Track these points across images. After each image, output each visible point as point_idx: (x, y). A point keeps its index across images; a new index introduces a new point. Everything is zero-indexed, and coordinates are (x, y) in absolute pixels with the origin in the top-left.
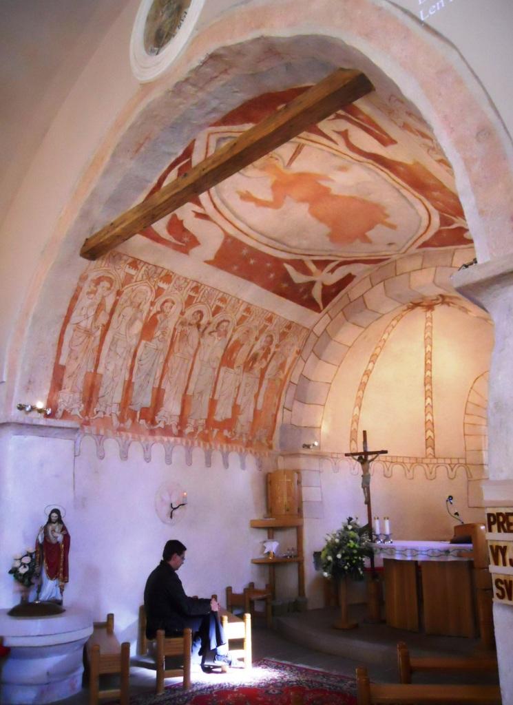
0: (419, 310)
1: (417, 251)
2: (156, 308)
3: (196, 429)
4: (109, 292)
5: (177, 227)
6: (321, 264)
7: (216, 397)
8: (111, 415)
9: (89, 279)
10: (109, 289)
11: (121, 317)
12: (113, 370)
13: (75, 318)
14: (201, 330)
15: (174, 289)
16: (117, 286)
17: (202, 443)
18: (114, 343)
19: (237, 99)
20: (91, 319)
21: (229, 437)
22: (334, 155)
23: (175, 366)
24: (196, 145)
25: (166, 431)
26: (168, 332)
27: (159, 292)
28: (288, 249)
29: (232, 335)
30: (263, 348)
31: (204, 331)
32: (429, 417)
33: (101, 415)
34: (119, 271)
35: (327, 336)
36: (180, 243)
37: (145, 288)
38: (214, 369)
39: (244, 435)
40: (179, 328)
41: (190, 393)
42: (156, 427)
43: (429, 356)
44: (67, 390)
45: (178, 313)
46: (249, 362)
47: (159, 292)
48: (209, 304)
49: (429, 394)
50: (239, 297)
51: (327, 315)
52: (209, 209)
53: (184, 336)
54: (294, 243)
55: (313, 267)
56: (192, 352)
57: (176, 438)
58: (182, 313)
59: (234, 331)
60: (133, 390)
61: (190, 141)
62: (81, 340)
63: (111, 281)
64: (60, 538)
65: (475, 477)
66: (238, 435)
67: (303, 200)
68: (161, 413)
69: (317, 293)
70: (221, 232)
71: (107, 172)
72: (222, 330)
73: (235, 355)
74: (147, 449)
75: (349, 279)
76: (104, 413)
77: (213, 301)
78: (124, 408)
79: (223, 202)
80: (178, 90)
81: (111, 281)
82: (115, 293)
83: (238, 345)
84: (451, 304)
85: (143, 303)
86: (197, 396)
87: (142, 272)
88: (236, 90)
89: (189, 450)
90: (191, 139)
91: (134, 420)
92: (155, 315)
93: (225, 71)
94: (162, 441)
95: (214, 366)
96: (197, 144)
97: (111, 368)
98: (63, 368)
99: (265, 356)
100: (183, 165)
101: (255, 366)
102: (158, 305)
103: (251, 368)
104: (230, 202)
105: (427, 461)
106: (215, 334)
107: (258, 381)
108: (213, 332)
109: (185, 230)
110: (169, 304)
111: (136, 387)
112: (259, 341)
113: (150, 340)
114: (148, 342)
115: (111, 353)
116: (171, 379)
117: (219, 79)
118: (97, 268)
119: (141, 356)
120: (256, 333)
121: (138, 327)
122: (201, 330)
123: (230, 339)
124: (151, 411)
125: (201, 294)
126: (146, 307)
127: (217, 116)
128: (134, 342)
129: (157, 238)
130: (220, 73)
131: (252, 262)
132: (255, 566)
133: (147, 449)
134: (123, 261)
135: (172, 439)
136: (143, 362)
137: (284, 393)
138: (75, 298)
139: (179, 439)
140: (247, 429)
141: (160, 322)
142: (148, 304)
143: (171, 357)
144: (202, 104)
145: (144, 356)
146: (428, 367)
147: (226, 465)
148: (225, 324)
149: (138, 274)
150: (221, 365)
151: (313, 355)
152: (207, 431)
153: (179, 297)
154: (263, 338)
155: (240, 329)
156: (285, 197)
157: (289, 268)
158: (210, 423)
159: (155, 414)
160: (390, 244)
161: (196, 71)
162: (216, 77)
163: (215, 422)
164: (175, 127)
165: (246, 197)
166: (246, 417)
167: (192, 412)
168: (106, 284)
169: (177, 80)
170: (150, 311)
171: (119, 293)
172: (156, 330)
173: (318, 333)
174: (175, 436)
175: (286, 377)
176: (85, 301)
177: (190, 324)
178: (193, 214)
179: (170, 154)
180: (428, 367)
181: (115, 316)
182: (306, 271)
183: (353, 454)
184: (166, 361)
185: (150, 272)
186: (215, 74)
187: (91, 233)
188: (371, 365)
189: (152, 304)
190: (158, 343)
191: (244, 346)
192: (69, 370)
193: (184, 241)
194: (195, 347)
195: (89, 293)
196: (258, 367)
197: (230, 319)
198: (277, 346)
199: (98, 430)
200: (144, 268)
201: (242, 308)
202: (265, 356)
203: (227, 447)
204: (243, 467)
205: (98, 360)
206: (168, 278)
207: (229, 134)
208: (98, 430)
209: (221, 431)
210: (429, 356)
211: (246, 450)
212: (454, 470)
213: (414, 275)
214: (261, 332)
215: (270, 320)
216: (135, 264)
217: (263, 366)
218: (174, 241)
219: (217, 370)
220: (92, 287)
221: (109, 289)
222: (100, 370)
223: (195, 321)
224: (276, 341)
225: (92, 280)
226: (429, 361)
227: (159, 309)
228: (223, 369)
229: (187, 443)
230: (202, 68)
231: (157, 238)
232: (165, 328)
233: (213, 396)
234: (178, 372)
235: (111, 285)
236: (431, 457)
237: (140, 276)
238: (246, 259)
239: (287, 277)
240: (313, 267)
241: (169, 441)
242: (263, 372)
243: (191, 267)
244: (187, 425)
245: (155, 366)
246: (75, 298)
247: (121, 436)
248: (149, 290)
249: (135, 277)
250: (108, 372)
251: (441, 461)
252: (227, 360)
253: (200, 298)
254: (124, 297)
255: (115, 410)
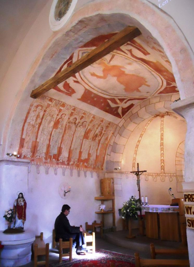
0: (158, 117)
1: (158, 95)
2: (59, 117)
3: (74, 162)
4: (41, 110)
5: (67, 86)
6: (121, 100)
7: (82, 150)
8: (42, 157)
9: (34, 106)
10: (41, 109)
11: (46, 120)
12: (43, 140)
13: (28, 120)
14: (76, 125)
15: (66, 110)
16: (44, 108)
17: (76, 168)
18: (43, 130)
19: (90, 37)
20: (34, 121)
21: (87, 165)
22: (126, 59)
23: (66, 138)
24: (74, 55)
25: (63, 163)
26: (64, 126)
27: (60, 110)
28: (109, 94)
29: (88, 127)
30: (100, 132)
31: (77, 125)
32: (162, 158)
33: (38, 157)
34: (45, 103)
35: (124, 127)
36: (68, 92)
37: (55, 109)
38: (81, 140)
39: (92, 165)
40: (68, 124)
41: (72, 149)
42: (59, 162)
43: (162, 135)
44: (26, 148)
45: (67, 119)
46: (94, 137)
47: (60, 110)
48: (79, 115)
49: (162, 149)
50: (90, 113)
51: (124, 119)
52: (79, 79)
53: (70, 127)
54: (111, 92)
55: (118, 101)
56: (73, 133)
57: (67, 166)
58: (69, 119)
59: (89, 125)
60: (50, 148)
61: (72, 53)
62: (31, 129)
63: (42, 106)
64: (23, 204)
65: (180, 181)
66: (90, 165)
67: (114, 76)
68: (61, 157)
69: (120, 111)
70: (84, 88)
71: (40, 65)
72: (84, 125)
73: (89, 134)
74: (55, 170)
75: (132, 106)
76: (39, 157)
77: (81, 114)
78: (47, 154)
79: (84, 76)
80: (67, 34)
81: (42, 106)
82: (43, 111)
83: (90, 131)
84: (171, 115)
85: (54, 115)
86: (74, 150)
87: (54, 103)
88: (89, 34)
89: (71, 170)
90: (72, 53)
91: (51, 159)
92: (59, 119)
93: (85, 27)
94: (61, 167)
95: (81, 139)
96: (75, 54)
97: (42, 139)
98: (24, 139)
99: (100, 135)
100: (69, 62)
101: (96, 138)
102: (60, 116)
103: (95, 139)
104: (87, 77)
105: (162, 175)
106: (81, 127)
107: (97, 144)
108: (81, 126)
109: (70, 87)
110: (64, 115)
111: (51, 147)
112: (98, 129)
113: (57, 129)
114: (56, 130)
115: (42, 134)
116: (65, 144)
117: (83, 30)
118: (37, 101)
119: (53, 135)
120: (97, 126)
121: (52, 124)
122: (76, 125)
123: (87, 128)
124: (57, 156)
125: (76, 111)
126: (55, 116)
127: (82, 44)
128: (51, 129)
129: (59, 90)
130: (83, 28)
131: (95, 99)
132: (96, 214)
133: (55, 170)
134: (46, 99)
135: (65, 166)
136: (54, 137)
137: (107, 149)
138: (28, 113)
139: (68, 166)
140: (93, 162)
141: (60, 122)
142: (56, 115)
143: (65, 135)
144: (76, 39)
145: (54, 135)
146: (162, 139)
147: (86, 176)
148: (85, 123)
149: (52, 104)
150: (84, 138)
151: (118, 134)
152: (78, 163)
153: (68, 113)
154: (99, 128)
155: (91, 124)
156: (108, 74)
157: (109, 101)
158: (79, 160)
159: (59, 157)
160: (148, 92)
161: (74, 27)
162: (82, 29)
163: (81, 160)
164: (66, 48)
165: (93, 75)
166: (93, 158)
167: (72, 156)
168: (40, 108)
169: (67, 30)
170: (57, 118)
171: (45, 111)
172: (59, 125)
173: (120, 126)
174: (66, 165)
175: (108, 143)
176: (32, 114)
177: (72, 123)
178: (73, 81)
179: (64, 58)
180: (162, 139)
181: (44, 120)
182: (116, 103)
183: (133, 172)
184: (63, 137)
185: (57, 103)
186: (81, 28)
187: (34, 88)
188: (140, 138)
189: (58, 115)
190: (60, 130)
191: (92, 131)
192: (26, 140)
193: (70, 91)
194: (74, 131)
195: (33, 111)
196: (97, 139)
197: (87, 121)
198: (105, 131)
199: (37, 163)
200: (54, 102)
201: (92, 117)
202: (100, 135)
203: (86, 169)
204: (92, 177)
205: (37, 136)
206: (63, 105)
207: (87, 51)
208: (37, 163)
209: (84, 163)
210: (162, 135)
211: (93, 171)
212: (172, 178)
213: (156, 104)
214: (99, 126)
215: (102, 121)
216: (51, 100)
217: (100, 139)
218: (66, 91)
219: (82, 140)
220: (35, 109)
221: (41, 109)
222: (38, 140)
223: (74, 122)
224: (104, 129)
225: (35, 106)
226: (162, 137)
227: (60, 117)
228: (84, 140)
229: (71, 168)
230: (77, 26)
231: (59, 90)
232: (63, 124)
233: (81, 150)
234: (67, 141)
235: (42, 108)
236: (163, 173)
237: (53, 105)
238: (93, 98)
239: (109, 105)
240: (118, 101)
241: (64, 167)
242: (99, 141)
243: (72, 101)
244: (71, 161)
245: (59, 138)
246: (28, 113)
247: (46, 165)
248: (56, 110)
249: (51, 105)
250: (41, 141)
251: (167, 175)
252: (86, 136)
253: (76, 113)
254: (47, 112)
255: (43, 155)
